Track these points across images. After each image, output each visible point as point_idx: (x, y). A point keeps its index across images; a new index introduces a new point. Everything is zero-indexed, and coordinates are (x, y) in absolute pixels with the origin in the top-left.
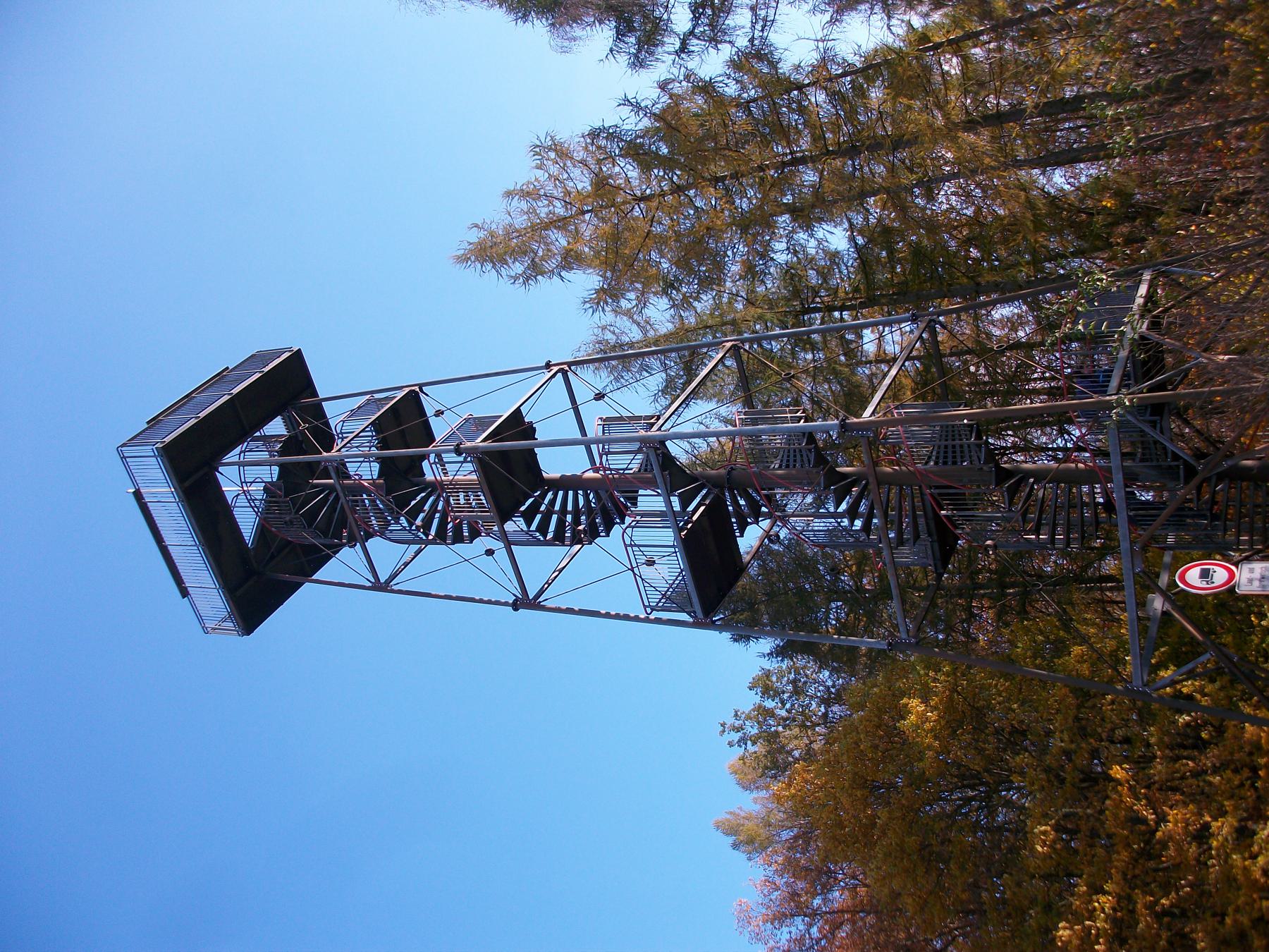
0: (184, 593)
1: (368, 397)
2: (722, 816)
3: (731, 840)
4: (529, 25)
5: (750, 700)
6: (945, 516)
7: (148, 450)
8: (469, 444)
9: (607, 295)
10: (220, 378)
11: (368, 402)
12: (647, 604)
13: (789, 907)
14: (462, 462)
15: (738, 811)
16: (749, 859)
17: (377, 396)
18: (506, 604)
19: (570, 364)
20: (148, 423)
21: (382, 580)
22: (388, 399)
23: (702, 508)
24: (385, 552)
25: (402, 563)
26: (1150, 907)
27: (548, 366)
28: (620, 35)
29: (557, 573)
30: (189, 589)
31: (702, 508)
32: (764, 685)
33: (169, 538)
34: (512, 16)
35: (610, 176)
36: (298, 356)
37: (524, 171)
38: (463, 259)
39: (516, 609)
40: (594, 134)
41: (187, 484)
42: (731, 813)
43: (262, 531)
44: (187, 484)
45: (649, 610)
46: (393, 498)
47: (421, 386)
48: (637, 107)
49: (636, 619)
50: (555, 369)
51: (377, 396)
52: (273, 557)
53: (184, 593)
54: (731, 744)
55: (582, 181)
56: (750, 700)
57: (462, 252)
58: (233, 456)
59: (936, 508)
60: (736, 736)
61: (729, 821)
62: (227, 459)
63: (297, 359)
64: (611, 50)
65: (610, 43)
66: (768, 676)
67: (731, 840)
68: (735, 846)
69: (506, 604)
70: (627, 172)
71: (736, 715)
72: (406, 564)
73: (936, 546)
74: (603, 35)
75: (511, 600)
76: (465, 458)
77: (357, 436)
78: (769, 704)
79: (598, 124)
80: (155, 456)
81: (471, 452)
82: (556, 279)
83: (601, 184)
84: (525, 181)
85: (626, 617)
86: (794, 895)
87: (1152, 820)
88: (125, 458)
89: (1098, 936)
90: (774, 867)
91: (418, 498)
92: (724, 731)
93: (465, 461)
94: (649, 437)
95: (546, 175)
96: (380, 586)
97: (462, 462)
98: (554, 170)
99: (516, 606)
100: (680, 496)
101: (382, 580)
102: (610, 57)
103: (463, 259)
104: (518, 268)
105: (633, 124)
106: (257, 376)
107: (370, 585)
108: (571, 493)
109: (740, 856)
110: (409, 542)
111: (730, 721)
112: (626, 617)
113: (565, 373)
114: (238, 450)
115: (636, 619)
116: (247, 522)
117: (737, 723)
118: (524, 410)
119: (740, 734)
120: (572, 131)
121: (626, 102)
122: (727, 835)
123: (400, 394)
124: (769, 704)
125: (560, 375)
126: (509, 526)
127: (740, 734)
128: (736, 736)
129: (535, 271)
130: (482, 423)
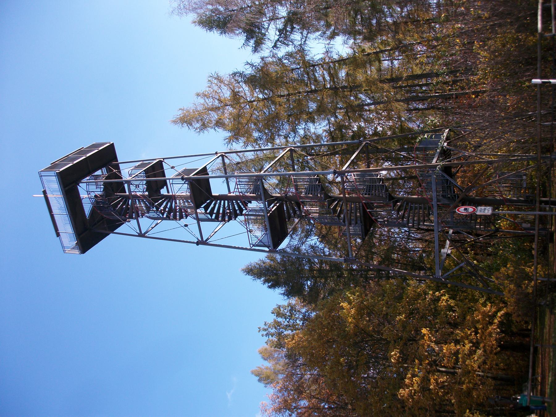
0: (58, 235)
1: (141, 162)
2: (255, 368)
3: (258, 378)
4: (212, 32)
5: (271, 318)
6: (369, 211)
7: (52, 173)
8: (186, 177)
9: (230, 140)
10: (81, 152)
11: (142, 164)
12: (251, 243)
13: (282, 406)
14: (183, 184)
15: (261, 367)
16: (266, 387)
17: (144, 162)
18: (193, 243)
19: (225, 153)
20: (51, 164)
21: (143, 233)
22: (150, 163)
23: (275, 207)
24: (145, 223)
25: (151, 227)
26: (436, 380)
27: (216, 153)
28: (248, 39)
29: (214, 233)
30: (60, 234)
31: (275, 207)
32: (278, 313)
33: (55, 211)
34: (205, 29)
35: (239, 92)
36: (112, 145)
37: (203, 87)
38: (175, 122)
39: (198, 245)
40: (234, 74)
41: (67, 188)
42: (258, 367)
43: (93, 212)
44: (67, 188)
45: (252, 246)
46: (151, 199)
47: (164, 159)
48: (252, 65)
49: (246, 249)
50: (219, 154)
51: (144, 162)
52: (95, 224)
53: (58, 235)
54: (263, 335)
55: (227, 94)
56: (271, 318)
57: (175, 119)
58: (85, 180)
59: (365, 208)
60: (265, 333)
61: (256, 370)
62: (83, 181)
63: (111, 147)
64: (244, 44)
65: (243, 42)
66: (279, 308)
67: (258, 378)
68: (260, 380)
69: (193, 243)
70: (245, 89)
71: (265, 324)
72: (153, 228)
73: (363, 227)
74: (241, 38)
75: (196, 241)
76: (185, 182)
77: (137, 175)
78: (280, 319)
79: (235, 71)
80: (55, 176)
81: (187, 179)
82: (213, 130)
83: (235, 96)
84: (205, 90)
85: (242, 249)
86: (286, 401)
87: (437, 350)
88: (41, 176)
89: (415, 393)
90: (277, 389)
91: (160, 201)
92: (260, 331)
93: (185, 183)
94: (260, 175)
95: (212, 90)
96: (141, 235)
97: (183, 184)
98: (216, 88)
99: (198, 243)
100: (268, 201)
101: (143, 233)
102: (243, 47)
103: (175, 122)
104: (198, 125)
105: (249, 71)
106: (97, 151)
107: (137, 234)
108: (222, 202)
109: (262, 385)
110: (155, 219)
111: (263, 326)
112: (242, 249)
113: (222, 156)
114: (88, 178)
115: (246, 249)
116: (87, 208)
117: (266, 327)
118: (208, 167)
119: (266, 332)
120: (225, 72)
121: (248, 63)
122: (257, 376)
123: (155, 162)
124: (280, 319)
125: (221, 158)
126: (198, 211)
127: (266, 332)
128: (265, 333)
129: (204, 126)
130: (192, 170)
